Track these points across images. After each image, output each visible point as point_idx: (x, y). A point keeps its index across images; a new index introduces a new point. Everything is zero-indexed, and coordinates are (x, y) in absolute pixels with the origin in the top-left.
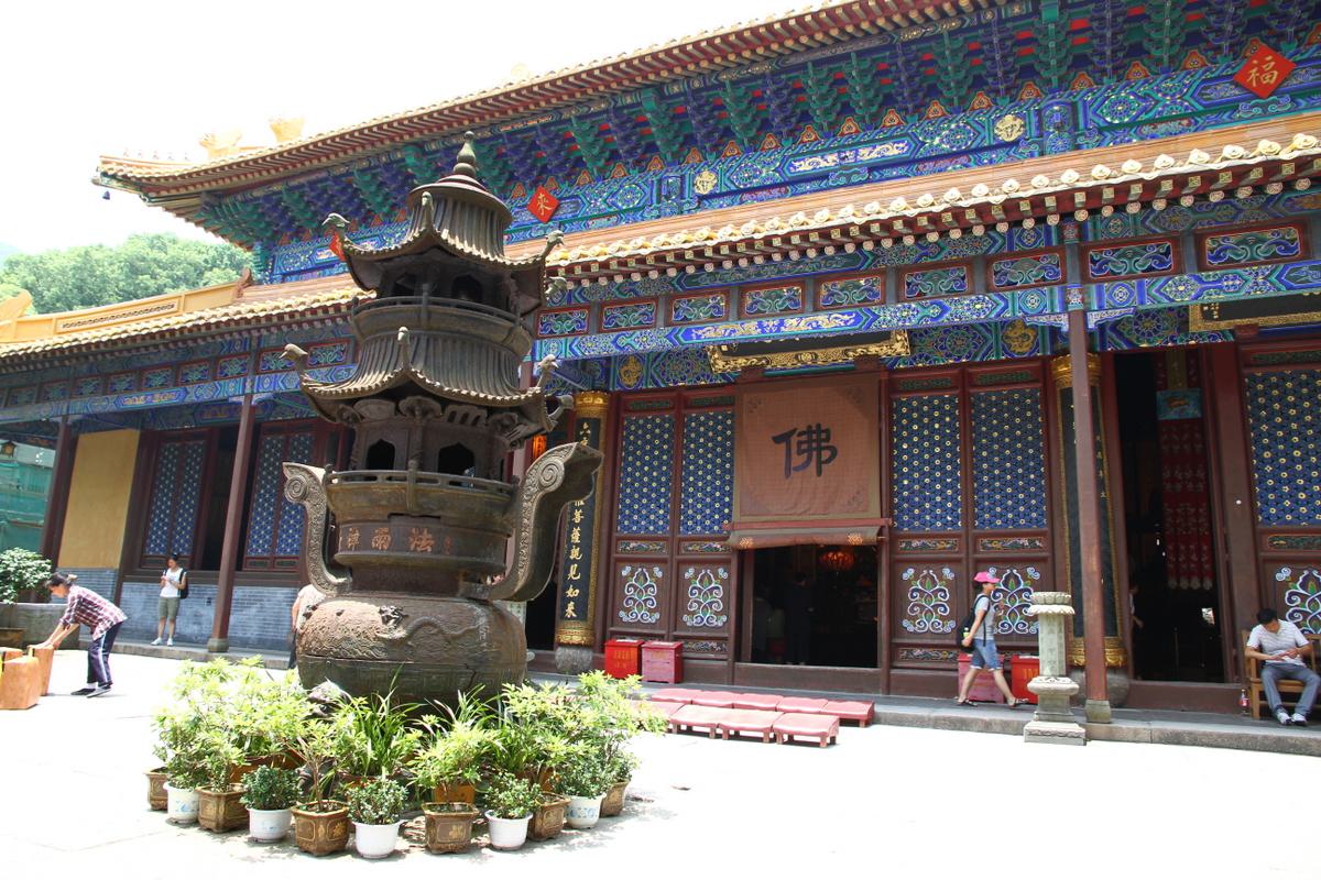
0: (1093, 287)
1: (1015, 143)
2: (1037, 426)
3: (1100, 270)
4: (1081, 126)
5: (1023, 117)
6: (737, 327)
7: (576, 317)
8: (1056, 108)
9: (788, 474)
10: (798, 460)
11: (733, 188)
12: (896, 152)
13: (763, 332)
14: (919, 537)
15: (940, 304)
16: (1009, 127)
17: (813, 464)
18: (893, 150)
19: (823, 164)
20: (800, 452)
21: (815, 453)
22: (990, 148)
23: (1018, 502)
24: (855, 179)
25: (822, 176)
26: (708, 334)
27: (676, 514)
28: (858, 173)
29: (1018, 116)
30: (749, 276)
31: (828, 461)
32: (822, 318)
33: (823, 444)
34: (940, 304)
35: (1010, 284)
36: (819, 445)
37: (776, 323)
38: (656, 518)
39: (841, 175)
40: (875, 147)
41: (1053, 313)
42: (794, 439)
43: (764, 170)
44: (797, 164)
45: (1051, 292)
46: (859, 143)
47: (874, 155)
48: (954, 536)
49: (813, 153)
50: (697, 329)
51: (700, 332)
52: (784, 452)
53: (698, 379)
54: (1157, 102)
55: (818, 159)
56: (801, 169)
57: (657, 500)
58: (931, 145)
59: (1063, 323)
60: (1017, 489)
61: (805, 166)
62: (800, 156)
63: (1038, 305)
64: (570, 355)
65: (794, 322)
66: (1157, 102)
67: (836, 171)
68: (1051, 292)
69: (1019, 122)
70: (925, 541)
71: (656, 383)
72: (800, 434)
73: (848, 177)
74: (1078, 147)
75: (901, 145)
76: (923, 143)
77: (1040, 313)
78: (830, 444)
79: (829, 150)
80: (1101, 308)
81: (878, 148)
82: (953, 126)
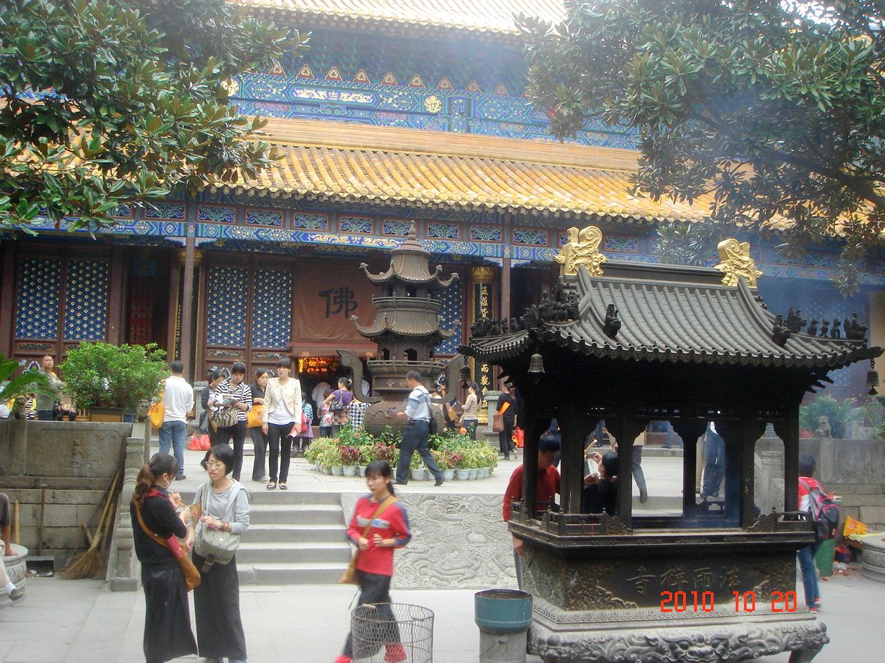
0: (515, 247)
1: (435, 115)
2: (460, 300)
3: (517, 239)
4: (472, 115)
5: (441, 100)
6: (336, 237)
7: (226, 212)
8: (460, 101)
9: (327, 317)
10: (334, 308)
11: (251, 97)
12: (365, 101)
13: (351, 242)
14: (219, 348)
15: (446, 244)
16: (433, 104)
17: (343, 310)
18: (363, 99)
19: (316, 96)
20: (335, 303)
21: (344, 305)
22: (421, 114)
23: (35, 313)
24: (337, 113)
25: (316, 104)
26: (318, 239)
27: (249, 336)
28: (340, 109)
29: (439, 98)
30: (343, 208)
31: (353, 309)
32: (385, 241)
33: (349, 300)
34: (446, 244)
35: (478, 238)
36: (347, 300)
37: (359, 239)
38: (236, 336)
39: (328, 107)
40: (351, 94)
41: (497, 257)
42: (332, 295)
43: (275, 90)
44: (298, 92)
45: (497, 246)
46: (342, 88)
47: (350, 99)
48: (240, 349)
49: (310, 87)
50: (311, 235)
51: (313, 237)
52: (325, 302)
53: (268, 249)
54: (511, 112)
55: (313, 92)
56: (301, 96)
57: (235, 324)
58: (387, 102)
59: (501, 262)
60: (43, 295)
61: (303, 94)
62: (301, 86)
63: (488, 249)
64: (224, 236)
65: (370, 240)
66: (511, 112)
67: (325, 104)
68: (497, 246)
69: (439, 102)
70: (223, 351)
71: (239, 249)
72: (335, 292)
73: (333, 110)
74: (469, 131)
75: (368, 97)
76: (382, 100)
77: (492, 257)
78: (353, 300)
79: (323, 88)
80: (517, 258)
81: (354, 95)
82: (401, 94)
